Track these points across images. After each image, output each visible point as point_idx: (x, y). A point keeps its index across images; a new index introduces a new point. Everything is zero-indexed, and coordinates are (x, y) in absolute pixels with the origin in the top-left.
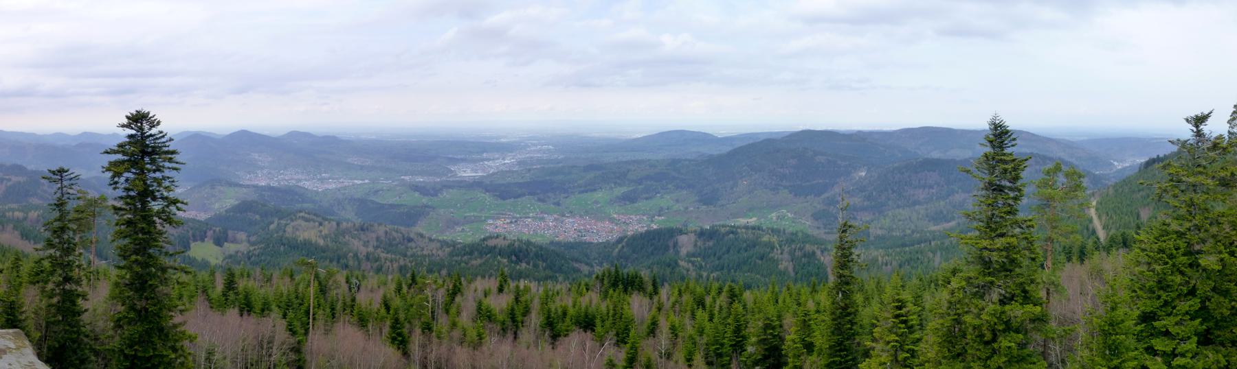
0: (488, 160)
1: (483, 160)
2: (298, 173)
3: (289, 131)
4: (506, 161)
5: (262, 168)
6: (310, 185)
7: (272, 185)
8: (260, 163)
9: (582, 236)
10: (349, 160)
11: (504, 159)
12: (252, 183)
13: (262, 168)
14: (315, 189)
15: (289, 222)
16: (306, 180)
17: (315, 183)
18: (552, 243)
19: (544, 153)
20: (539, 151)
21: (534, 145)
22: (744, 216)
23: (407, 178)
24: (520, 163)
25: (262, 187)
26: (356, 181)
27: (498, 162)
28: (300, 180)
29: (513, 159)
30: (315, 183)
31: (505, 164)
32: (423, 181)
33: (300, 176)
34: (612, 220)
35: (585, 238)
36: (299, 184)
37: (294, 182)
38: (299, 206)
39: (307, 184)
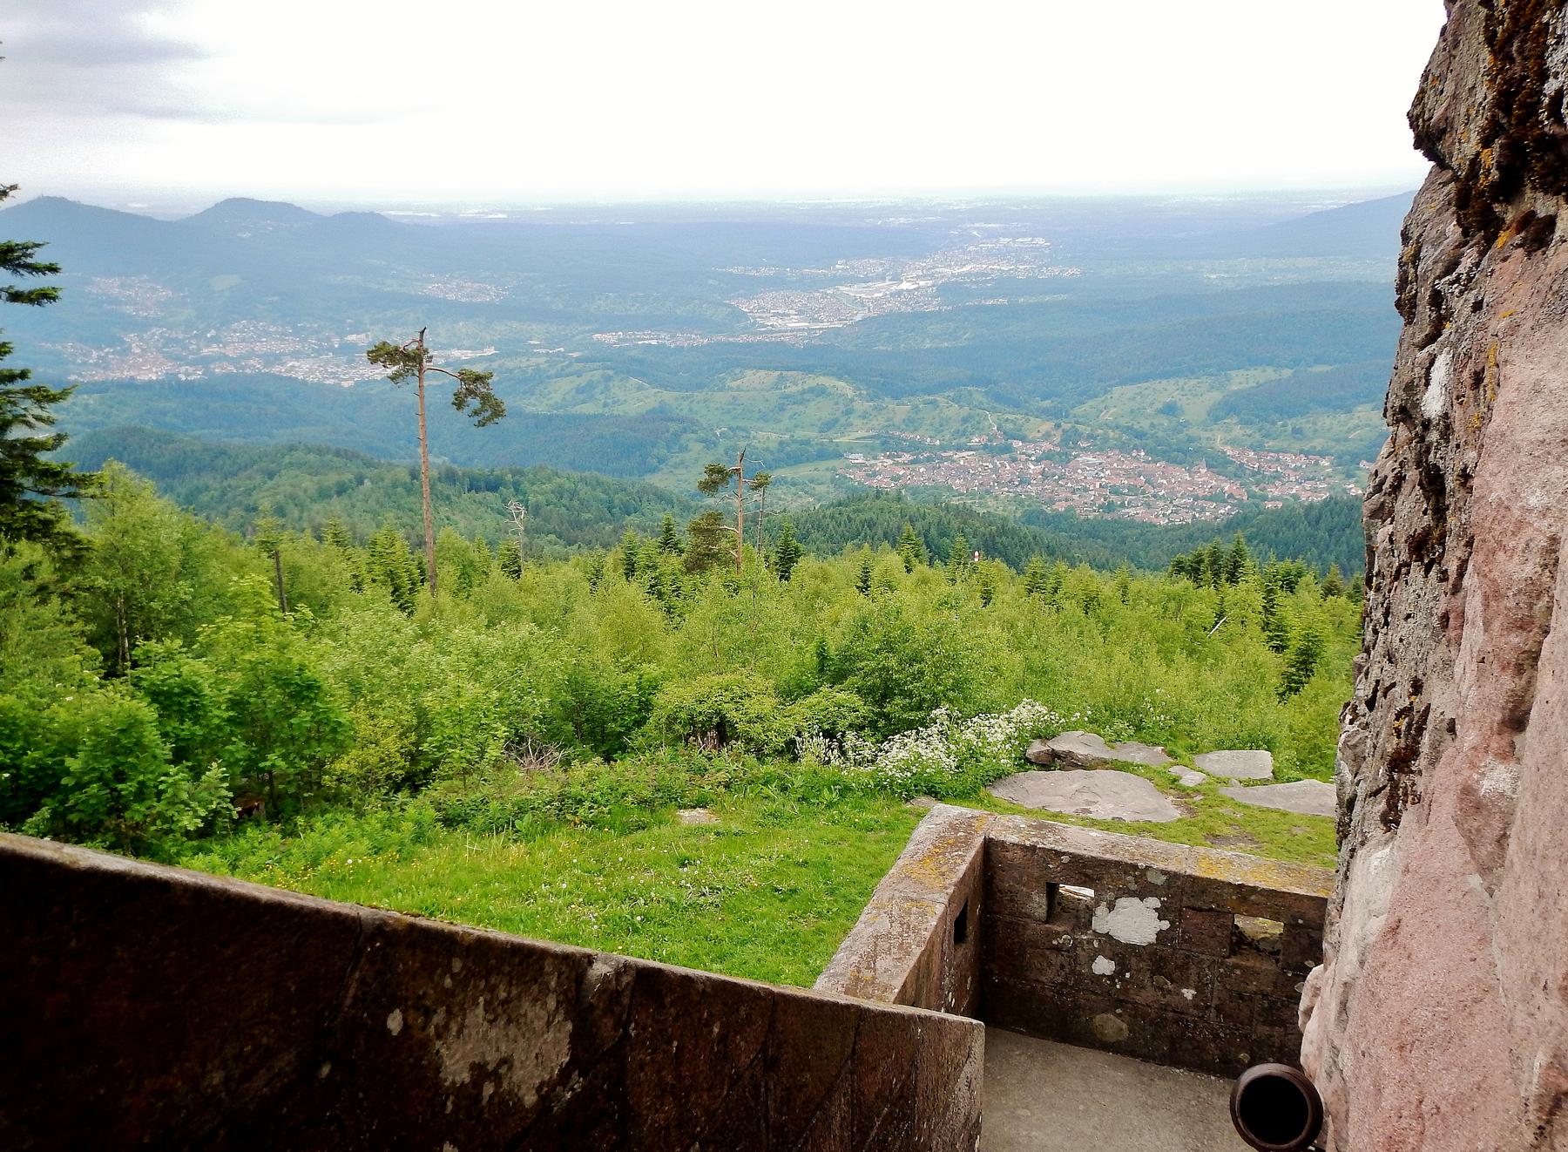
0: (853, 280)
1: (836, 281)
2: (267, 333)
3: (226, 198)
4: (905, 286)
5: (142, 326)
6: (311, 371)
7: (183, 378)
8: (129, 309)
9: (1122, 506)
10: (432, 289)
11: (897, 279)
12: (116, 375)
13: (142, 326)
14: (331, 382)
15: (258, 479)
16: (296, 355)
17: (327, 362)
18: (1031, 518)
19: (1020, 261)
20: (1003, 254)
21: (992, 235)
22: (992, 297)
23: (610, 338)
24: (948, 290)
25: (149, 385)
26: (456, 353)
27: (880, 289)
28: (278, 358)
29: (924, 277)
30: (327, 362)
31: (900, 293)
32: (659, 346)
33: (276, 346)
34: (1218, 464)
35: (1132, 511)
36: (276, 369)
37: (256, 364)
38: (283, 436)
39: (302, 369)
